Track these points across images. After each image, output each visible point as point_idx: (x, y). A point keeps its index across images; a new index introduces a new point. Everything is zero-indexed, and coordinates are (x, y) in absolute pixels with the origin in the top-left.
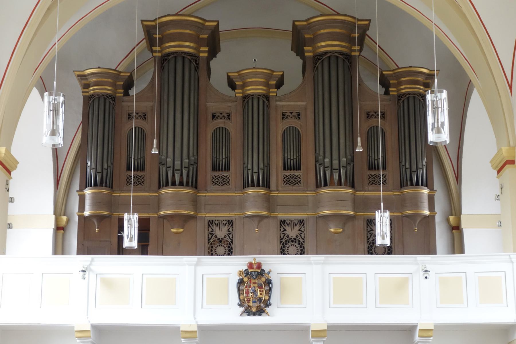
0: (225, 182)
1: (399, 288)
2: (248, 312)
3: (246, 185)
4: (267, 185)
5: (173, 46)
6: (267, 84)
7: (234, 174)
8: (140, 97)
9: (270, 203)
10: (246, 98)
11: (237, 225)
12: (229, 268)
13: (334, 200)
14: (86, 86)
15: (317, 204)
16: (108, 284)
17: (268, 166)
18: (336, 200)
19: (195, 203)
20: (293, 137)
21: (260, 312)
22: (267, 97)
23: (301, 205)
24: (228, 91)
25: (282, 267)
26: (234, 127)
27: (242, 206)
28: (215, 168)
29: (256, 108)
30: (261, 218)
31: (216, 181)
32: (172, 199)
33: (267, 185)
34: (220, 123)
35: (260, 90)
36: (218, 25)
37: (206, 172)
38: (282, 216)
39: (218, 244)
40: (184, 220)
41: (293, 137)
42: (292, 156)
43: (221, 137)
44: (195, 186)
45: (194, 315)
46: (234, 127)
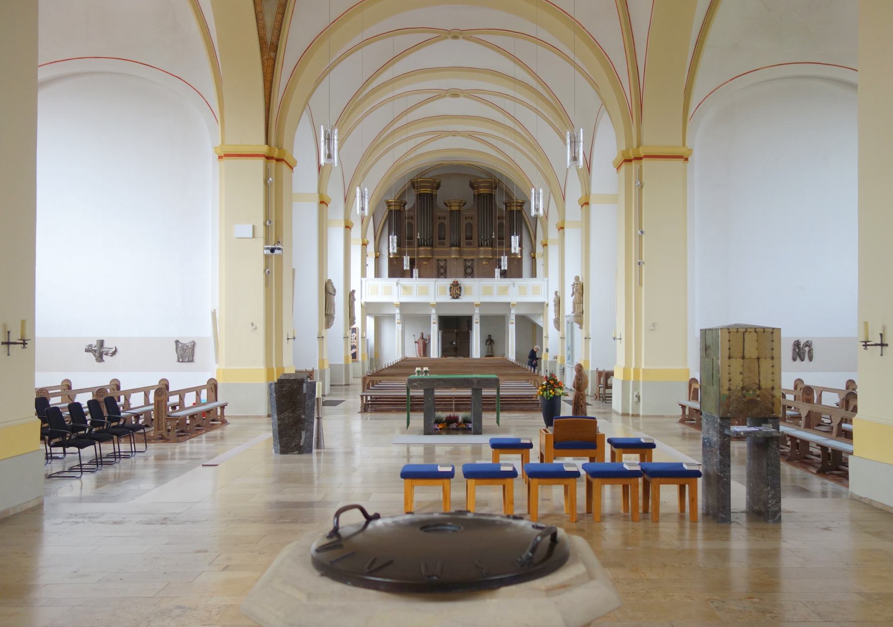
0: (444, 244)
1: (505, 290)
2: (453, 298)
3: (452, 246)
4: (459, 246)
5: (423, 191)
6: (460, 206)
7: (447, 241)
8: (409, 210)
9: (460, 253)
10: (451, 211)
11: (448, 261)
12: (446, 282)
13: (484, 252)
14: (389, 206)
15: (478, 253)
16: (405, 288)
17: (460, 238)
18: (486, 252)
19: (432, 253)
20: (469, 227)
21: (457, 298)
22: (459, 211)
23: (472, 253)
24: (445, 207)
25: (465, 282)
26: (447, 222)
27: (450, 253)
28: (439, 239)
29: (456, 215)
30: (457, 259)
31: (440, 244)
32: (423, 252)
33: (459, 246)
34: (441, 221)
35: (457, 208)
36: (453, 469)
37: (436, 241)
38: (465, 257)
39: (441, 272)
40: (428, 259)
41: (469, 227)
42: (469, 234)
43: (442, 226)
44: (432, 246)
45: (226, 155)
46: (447, 222)
